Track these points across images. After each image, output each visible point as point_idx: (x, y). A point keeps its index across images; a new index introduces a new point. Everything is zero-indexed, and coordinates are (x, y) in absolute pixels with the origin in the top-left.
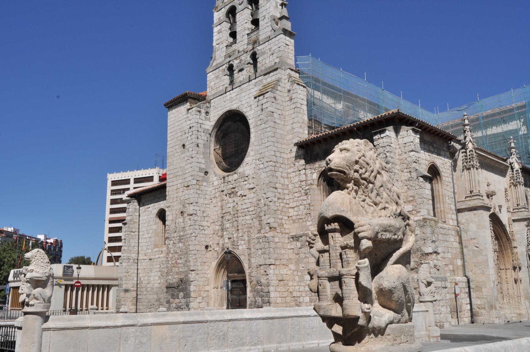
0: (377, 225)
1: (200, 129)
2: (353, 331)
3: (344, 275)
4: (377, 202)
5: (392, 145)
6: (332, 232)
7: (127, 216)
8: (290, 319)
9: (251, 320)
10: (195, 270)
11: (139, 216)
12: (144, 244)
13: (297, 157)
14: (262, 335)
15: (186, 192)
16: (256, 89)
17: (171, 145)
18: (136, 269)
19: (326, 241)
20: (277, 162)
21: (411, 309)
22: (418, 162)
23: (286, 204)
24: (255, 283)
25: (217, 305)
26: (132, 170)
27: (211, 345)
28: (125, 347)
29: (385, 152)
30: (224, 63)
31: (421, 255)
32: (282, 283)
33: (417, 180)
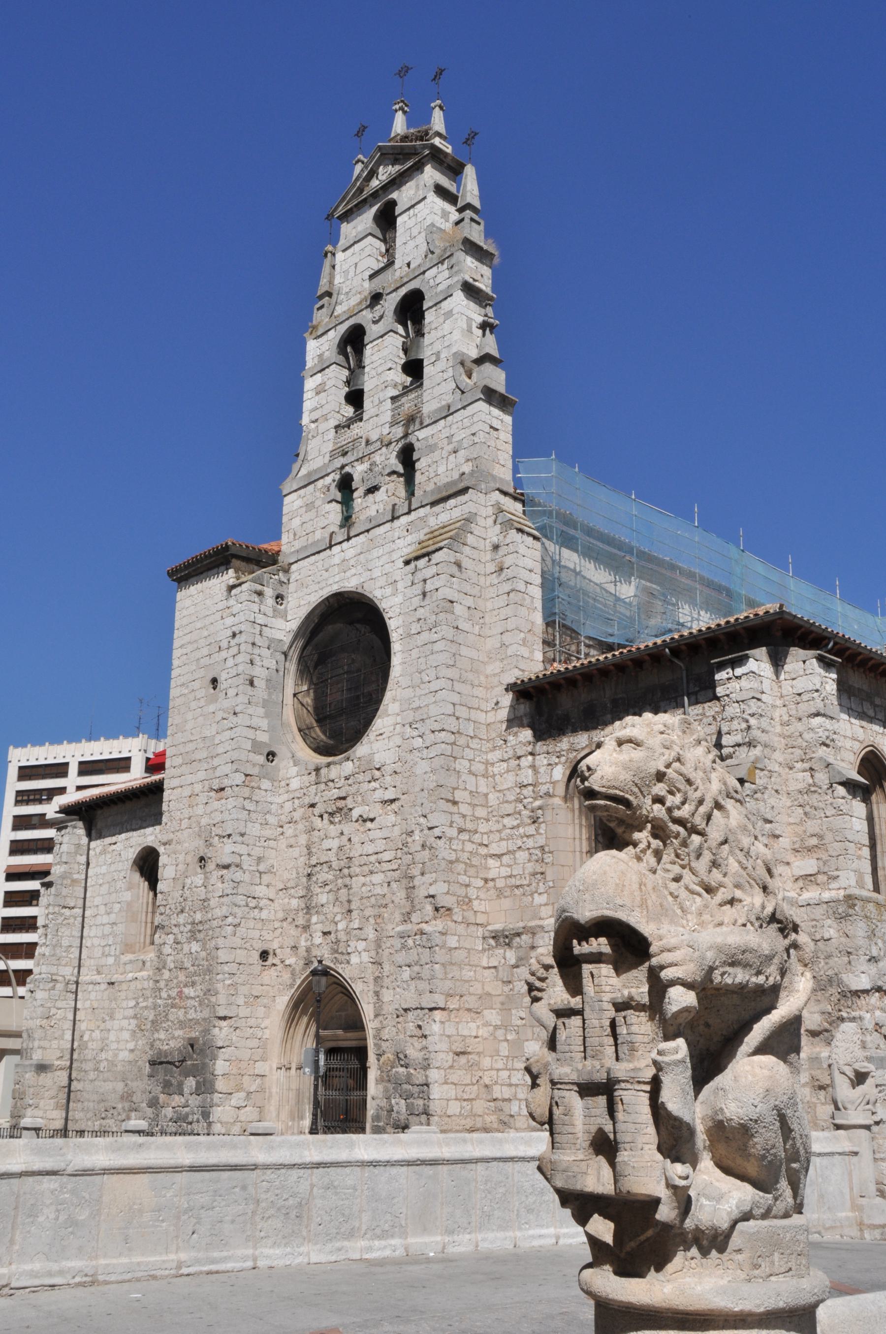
0: (710, 948)
1: (258, 640)
2: (642, 1238)
3: (619, 1082)
4: (713, 884)
5: (764, 697)
6: (590, 962)
7: (56, 864)
8: (480, 1167)
9: (375, 1166)
10: (230, 1018)
11: (88, 864)
12: (96, 942)
13: (513, 722)
14: (404, 1210)
15: (216, 805)
16: (410, 539)
17: (182, 680)
18: (72, 1010)
19: (574, 986)
20: (458, 732)
21: (800, 1179)
22: (831, 744)
23: (481, 844)
24: (391, 1057)
25: (284, 1115)
26: (74, 738)
27: (262, 1234)
28: (29, 1232)
29: (746, 716)
30: (329, 471)
31: (838, 996)
32: (463, 1060)
33: (830, 791)
